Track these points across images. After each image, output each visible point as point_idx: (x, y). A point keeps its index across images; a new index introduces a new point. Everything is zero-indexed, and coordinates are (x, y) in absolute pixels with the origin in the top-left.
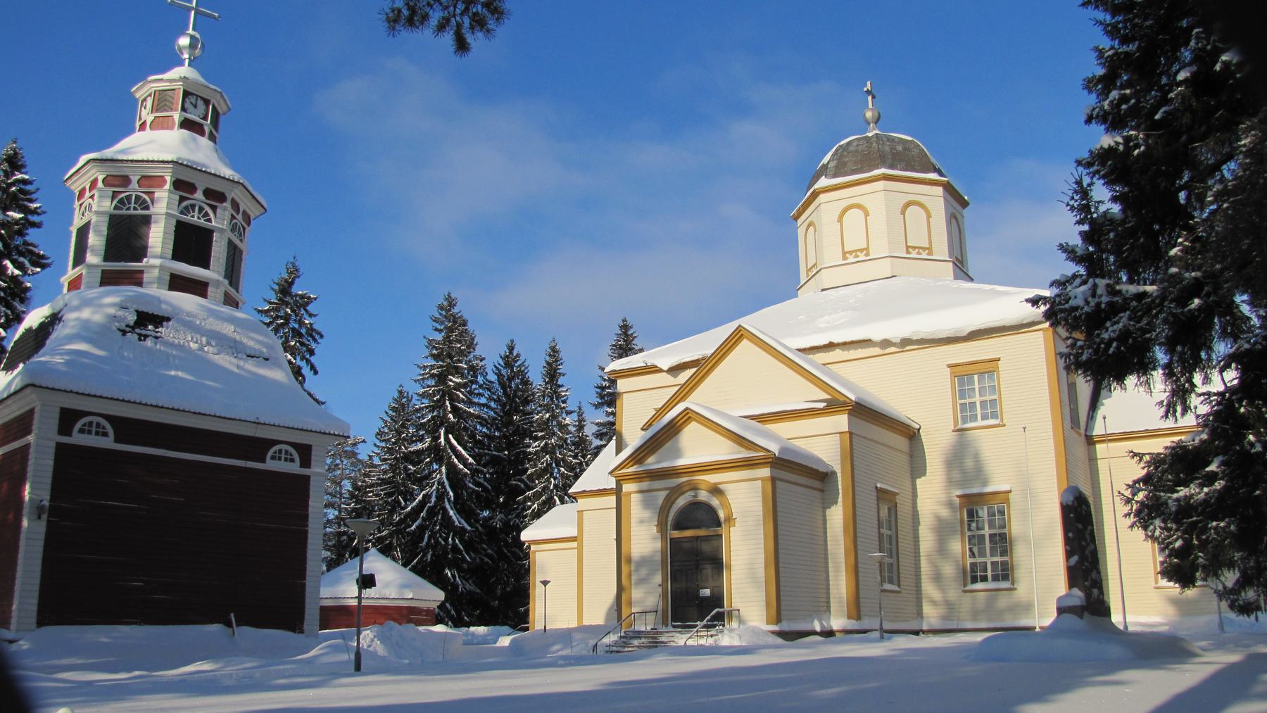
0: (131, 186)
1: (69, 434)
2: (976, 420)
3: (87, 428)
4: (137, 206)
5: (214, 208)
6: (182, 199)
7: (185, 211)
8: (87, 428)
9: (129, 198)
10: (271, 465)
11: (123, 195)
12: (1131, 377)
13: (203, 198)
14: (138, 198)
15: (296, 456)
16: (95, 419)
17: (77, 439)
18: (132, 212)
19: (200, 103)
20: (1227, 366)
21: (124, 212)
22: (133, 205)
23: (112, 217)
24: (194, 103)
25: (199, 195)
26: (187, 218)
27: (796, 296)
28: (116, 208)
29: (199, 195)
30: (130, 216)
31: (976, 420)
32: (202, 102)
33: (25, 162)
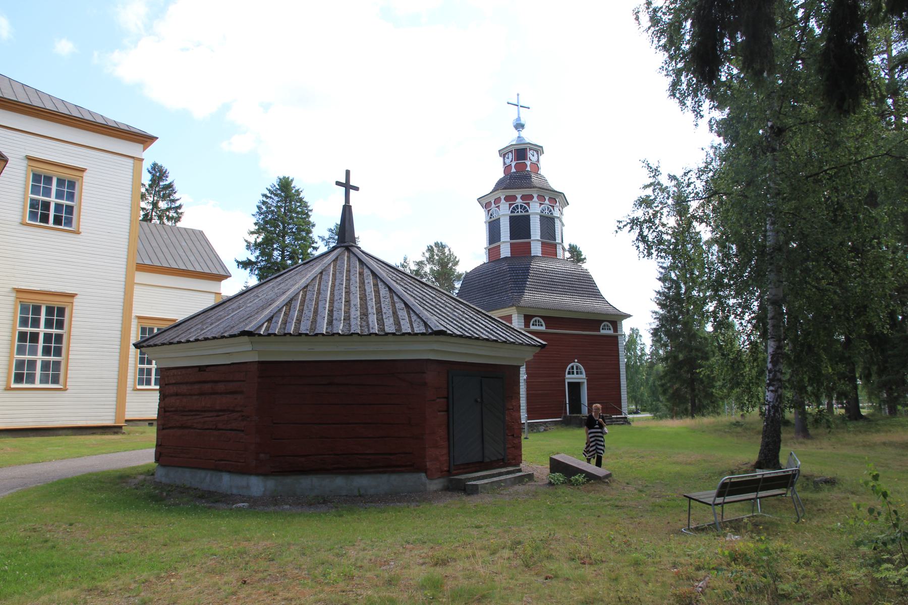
0: (517, 201)
2: (33, 382)
6: (510, 205)
10: (603, 332)
11: (514, 205)
12: (706, 104)
13: (521, 201)
14: (521, 206)
18: (520, 214)
19: (535, 153)
20: (840, 381)
21: (516, 214)
22: (519, 210)
23: (510, 217)
27: (201, 233)
28: (512, 212)
30: (519, 216)
31: (33, 382)
33: (330, 230)
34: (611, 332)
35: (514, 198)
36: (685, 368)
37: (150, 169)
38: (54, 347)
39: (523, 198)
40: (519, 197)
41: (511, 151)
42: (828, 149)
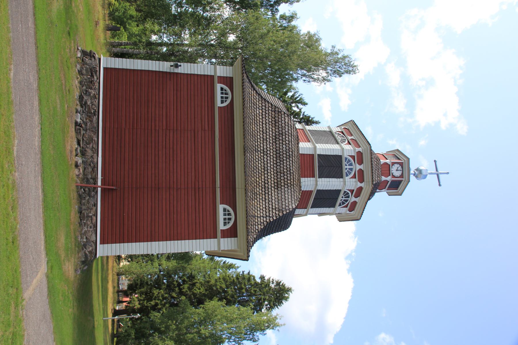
0: (357, 165)
1: (219, 82)
3: (224, 92)
4: (348, 169)
5: (354, 177)
6: (353, 157)
7: (346, 194)
8: (227, 213)
9: (351, 165)
10: (221, 207)
13: (358, 169)
14: (351, 169)
15: (228, 226)
16: (233, 217)
17: (218, 86)
18: (344, 167)
23: (340, 157)
24: (398, 169)
25: (358, 167)
26: (341, 194)
28: (346, 159)
29: (358, 167)
32: (401, 174)
34: (221, 226)
35: (361, 162)
36: (153, 284)
37: (301, 96)
38: (228, 220)
39: (361, 172)
40: (361, 167)
41: (402, 176)
42: (159, 306)
